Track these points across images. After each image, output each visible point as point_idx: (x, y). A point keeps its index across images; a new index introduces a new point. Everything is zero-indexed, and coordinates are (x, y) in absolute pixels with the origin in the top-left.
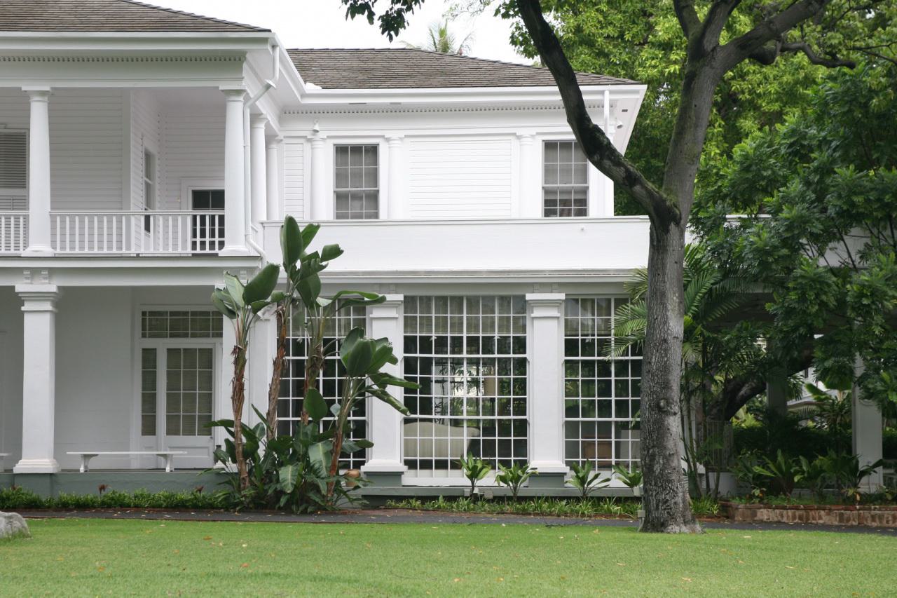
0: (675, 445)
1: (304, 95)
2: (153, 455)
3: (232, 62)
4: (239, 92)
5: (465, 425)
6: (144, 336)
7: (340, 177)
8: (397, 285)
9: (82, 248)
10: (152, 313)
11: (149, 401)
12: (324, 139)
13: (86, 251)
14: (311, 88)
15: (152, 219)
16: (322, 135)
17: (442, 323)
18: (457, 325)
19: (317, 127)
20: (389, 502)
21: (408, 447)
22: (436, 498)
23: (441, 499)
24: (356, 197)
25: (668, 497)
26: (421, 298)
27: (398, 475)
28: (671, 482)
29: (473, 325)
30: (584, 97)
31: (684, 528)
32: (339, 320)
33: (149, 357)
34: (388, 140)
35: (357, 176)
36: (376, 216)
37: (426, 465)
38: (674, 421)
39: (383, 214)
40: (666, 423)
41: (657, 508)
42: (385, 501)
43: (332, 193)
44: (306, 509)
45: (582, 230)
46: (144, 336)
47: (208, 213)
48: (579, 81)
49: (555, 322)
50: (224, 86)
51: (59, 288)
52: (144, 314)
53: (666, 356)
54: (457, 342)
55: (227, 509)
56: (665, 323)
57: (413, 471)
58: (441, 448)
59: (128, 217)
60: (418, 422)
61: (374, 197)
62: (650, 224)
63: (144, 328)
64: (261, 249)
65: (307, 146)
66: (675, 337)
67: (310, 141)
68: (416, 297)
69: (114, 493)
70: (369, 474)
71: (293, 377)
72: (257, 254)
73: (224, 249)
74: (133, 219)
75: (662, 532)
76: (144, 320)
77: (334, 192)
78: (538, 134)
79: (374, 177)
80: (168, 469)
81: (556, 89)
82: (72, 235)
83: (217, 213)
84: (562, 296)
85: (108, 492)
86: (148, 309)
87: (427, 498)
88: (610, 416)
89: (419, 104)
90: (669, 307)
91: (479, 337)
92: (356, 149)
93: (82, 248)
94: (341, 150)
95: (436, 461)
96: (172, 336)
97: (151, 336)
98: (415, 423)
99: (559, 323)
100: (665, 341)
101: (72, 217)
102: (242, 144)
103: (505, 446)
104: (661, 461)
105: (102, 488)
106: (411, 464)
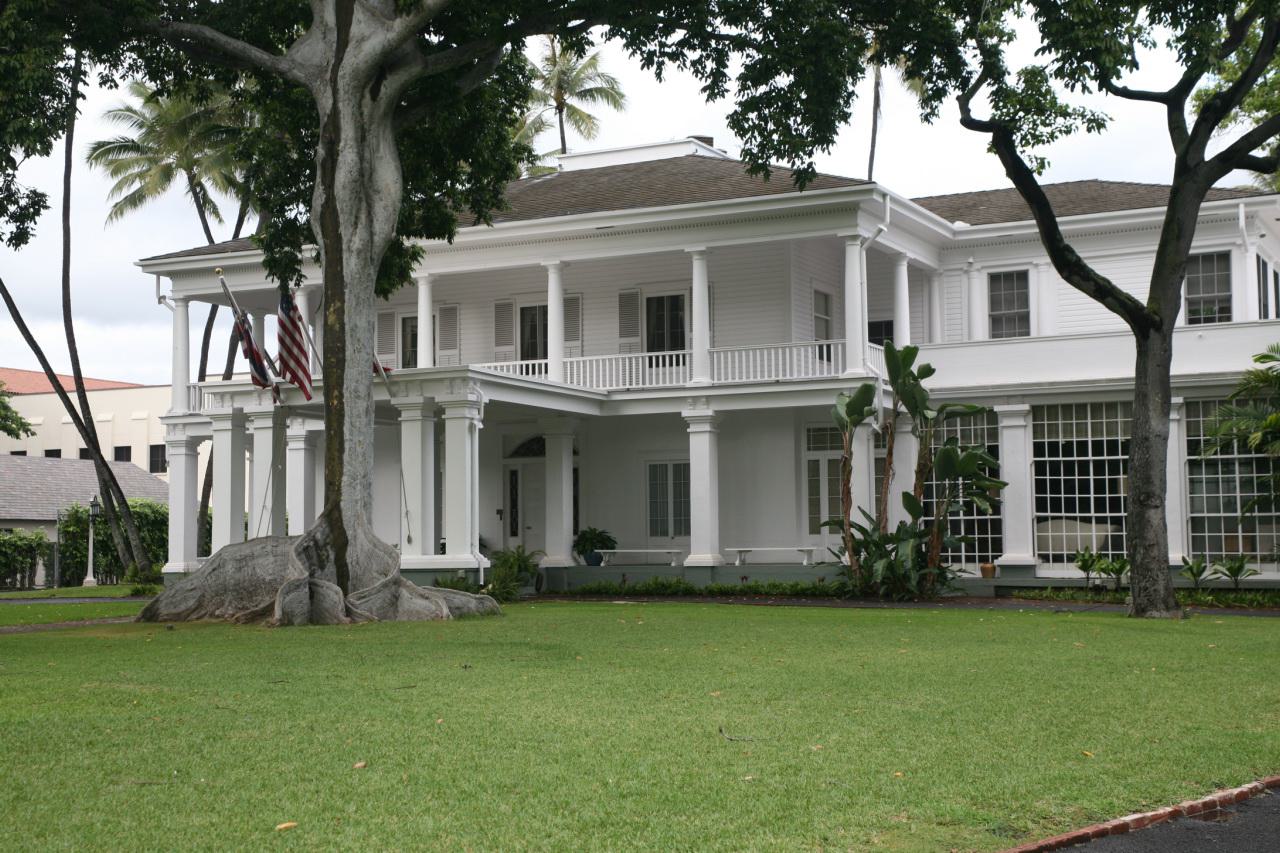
0: (1156, 535)
1: (955, 233)
2: (793, 551)
3: (850, 211)
4: (855, 237)
5: (1094, 521)
6: (809, 449)
7: (994, 303)
8: (1024, 396)
9: (741, 378)
10: (815, 430)
11: (814, 505)
12: (978, 270)
13: (737, 380)
14: (959, 225)
15: (832, 347)
16: (977, 266)
17: (1067, 431)
18: (1082, 430)
19: (971, 260)
20: (1016, 592)
21: (1041, 543)
22: (1045, 588)
23: (1049, 590)
24: (1010, 319)
25: (1148, 585)
26: (1063, 406)
27: (1032, 568)
28: (1149, 570)
29: (1096, 430)
30: (1061, 228)
31: (1164, 614)
32: (975, 430)
33: (814, 467)
34: (1037, 265)
35: (1010, 303)
36: (1028, 334)
37: (1058, 559)
38: (1156, 513)
39: (1034, 332)
40: (1147, 516)
41: (1139, 596)
42: (1012, 591)
43: (987, 318)
44: (904, 596)
45: (1200, 336)
46: (809, 449)
47: (530, 362)
48: (1055, 213)
49: (1022, 431)
50: (841, 233)
51: (716, 412)
52: (809, 430)
53: (1148, 452)
54: (1082, 448)
55: (839, 597)
56: (1147, 421)
57: (1046, 565)
58: (1071, 540)
59: (790, 348)
60: (1064, 520)
61: (1025, 319)
62: (1133, 339)
63: (809, 443)
64: (878, 372)
65: (964, 278)
66: (1157, 436)
67: (967, 272)
68: (1043, 407)
69: (756, 582)
70: (1004, 568)
71: (1201, 474)
72: (873, 375)
73: (846, 373)
74: (795, 351)
75: (1142, 617)
76: (809, 436)
77: (990, 316)
78: (983, 268)
79: (1024, 300)
80: (673, 564)
81: (1034, 222)
82: (748, 367)
83: (543, 362)
84: (1026, 407)
85: (751, 582)
86: (812, 426)
87: (1059, 587)
88: (1089, 512)
89: (1124, 225)
90: (1151, 408)
91: (1102, 441)
92: (1008, 276)
93: (741, 378)
94: (994, 279)
95: (1067, 555)
96: (832, 448)
97: (816, 449)
98: (1045, 523)
99: (1179, 426)
100: (1147, 439)
101: (784, 348)
102: (859, 281)
103: (983, 543)
104: (1142, 552)
105: (744, 578)
106: (1045, 558)
